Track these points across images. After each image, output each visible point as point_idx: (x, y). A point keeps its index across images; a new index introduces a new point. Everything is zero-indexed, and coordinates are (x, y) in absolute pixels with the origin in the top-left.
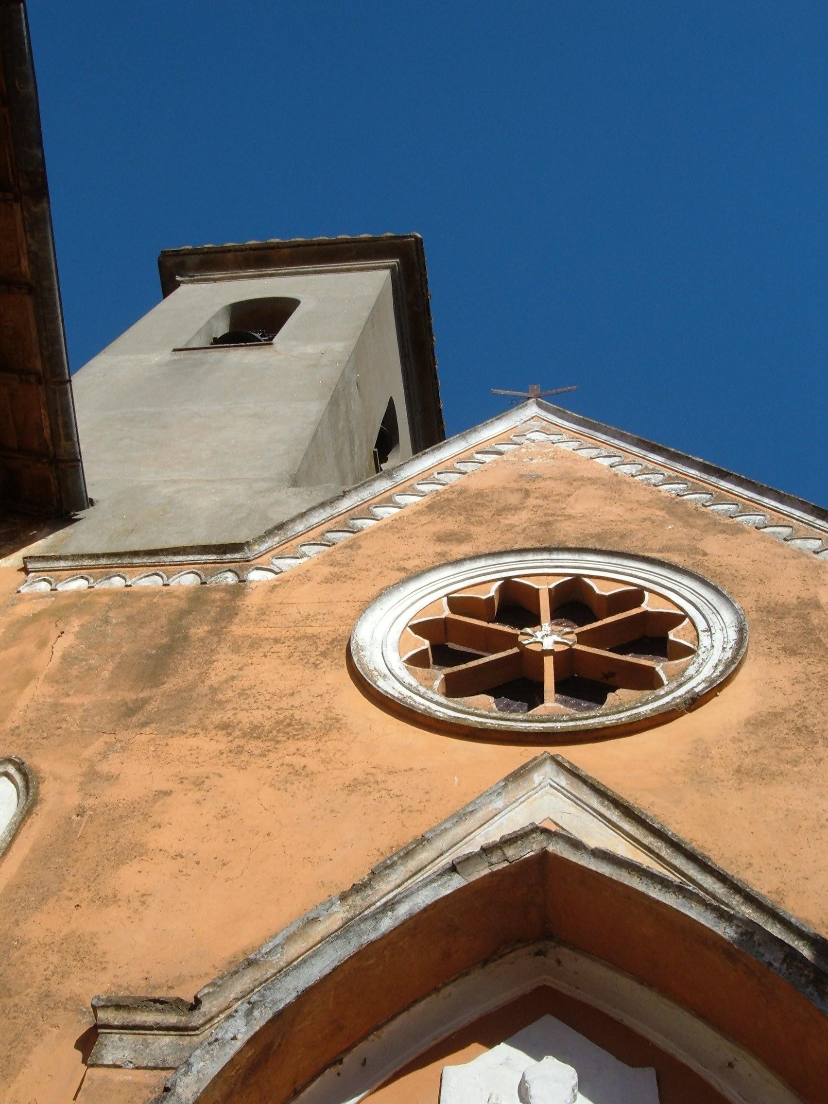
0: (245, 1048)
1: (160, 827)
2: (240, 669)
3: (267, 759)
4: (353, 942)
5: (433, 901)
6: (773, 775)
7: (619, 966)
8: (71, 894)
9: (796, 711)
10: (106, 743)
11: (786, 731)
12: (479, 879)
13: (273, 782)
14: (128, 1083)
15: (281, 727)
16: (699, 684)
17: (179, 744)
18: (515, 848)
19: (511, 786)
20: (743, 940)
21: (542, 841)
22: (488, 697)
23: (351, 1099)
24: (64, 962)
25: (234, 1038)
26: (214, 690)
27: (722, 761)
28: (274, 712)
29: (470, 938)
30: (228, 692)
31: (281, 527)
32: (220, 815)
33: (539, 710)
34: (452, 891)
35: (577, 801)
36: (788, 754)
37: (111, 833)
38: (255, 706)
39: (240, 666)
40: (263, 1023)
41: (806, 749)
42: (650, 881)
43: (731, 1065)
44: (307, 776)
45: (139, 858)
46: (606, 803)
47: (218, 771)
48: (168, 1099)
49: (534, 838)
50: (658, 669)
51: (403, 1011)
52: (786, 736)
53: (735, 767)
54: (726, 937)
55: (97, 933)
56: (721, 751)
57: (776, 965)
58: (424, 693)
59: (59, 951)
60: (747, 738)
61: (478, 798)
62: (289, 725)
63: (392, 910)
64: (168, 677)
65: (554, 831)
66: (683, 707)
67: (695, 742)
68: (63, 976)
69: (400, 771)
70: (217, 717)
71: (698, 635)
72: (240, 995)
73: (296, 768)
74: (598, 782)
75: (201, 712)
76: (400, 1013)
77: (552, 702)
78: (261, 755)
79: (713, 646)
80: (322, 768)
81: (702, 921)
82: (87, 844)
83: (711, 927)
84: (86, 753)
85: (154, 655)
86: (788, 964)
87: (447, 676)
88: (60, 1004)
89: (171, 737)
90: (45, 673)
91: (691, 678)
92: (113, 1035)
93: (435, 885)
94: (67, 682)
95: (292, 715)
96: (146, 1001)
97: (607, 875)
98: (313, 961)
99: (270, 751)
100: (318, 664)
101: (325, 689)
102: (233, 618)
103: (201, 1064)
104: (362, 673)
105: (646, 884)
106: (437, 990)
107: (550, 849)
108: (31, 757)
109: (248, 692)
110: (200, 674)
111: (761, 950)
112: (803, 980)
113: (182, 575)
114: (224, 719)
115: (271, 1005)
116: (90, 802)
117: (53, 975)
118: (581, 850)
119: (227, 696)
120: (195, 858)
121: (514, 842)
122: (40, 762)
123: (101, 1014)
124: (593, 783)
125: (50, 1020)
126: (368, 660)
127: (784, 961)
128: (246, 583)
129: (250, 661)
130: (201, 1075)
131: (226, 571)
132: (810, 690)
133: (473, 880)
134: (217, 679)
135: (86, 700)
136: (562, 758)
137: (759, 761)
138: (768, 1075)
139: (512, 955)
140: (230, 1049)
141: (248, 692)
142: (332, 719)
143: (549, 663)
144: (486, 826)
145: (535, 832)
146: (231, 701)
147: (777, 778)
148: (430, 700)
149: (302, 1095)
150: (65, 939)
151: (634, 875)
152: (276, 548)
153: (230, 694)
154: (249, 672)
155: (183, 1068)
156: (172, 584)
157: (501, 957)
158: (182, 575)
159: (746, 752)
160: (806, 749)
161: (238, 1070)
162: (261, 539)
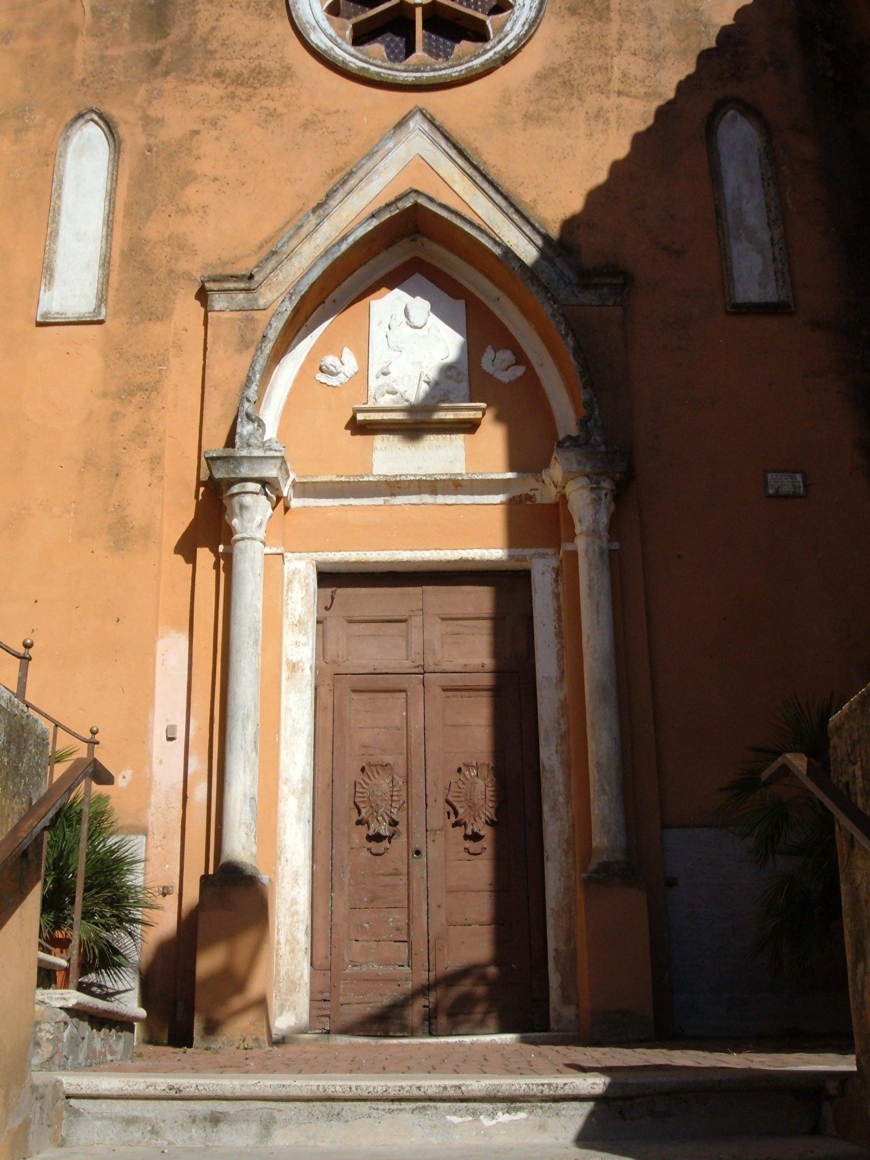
3: (250, 103)
14: (229, 319)
16: (511, 41)
19: (398, 132)
25: (286, 310)
33: (413, 59)
35: (434, 141)
40: (297, 302)
46: (449, 144)
50: (488, 22)
54: (497, 253)
58: (268, 1124)
61: (379, 142)
62: (259, 73)
63: (346, 240)
66: (499, 63)
68: (176, 260)
70: (213, 66)
72: (271, 271)
79: (524, 5)
80: (285, 111)
91: (506, 36)
93: (365, 225)
106: (365, 263)
107: (419, 201)
110: (191, 25)
114: (217, 68)
116: (152, 141)
122: (115, 111)
126: (302, 13)
136: (426, 111)
143: (419, 12)
148: (345, 51)
149: (309, 320)
150: (170, 237)
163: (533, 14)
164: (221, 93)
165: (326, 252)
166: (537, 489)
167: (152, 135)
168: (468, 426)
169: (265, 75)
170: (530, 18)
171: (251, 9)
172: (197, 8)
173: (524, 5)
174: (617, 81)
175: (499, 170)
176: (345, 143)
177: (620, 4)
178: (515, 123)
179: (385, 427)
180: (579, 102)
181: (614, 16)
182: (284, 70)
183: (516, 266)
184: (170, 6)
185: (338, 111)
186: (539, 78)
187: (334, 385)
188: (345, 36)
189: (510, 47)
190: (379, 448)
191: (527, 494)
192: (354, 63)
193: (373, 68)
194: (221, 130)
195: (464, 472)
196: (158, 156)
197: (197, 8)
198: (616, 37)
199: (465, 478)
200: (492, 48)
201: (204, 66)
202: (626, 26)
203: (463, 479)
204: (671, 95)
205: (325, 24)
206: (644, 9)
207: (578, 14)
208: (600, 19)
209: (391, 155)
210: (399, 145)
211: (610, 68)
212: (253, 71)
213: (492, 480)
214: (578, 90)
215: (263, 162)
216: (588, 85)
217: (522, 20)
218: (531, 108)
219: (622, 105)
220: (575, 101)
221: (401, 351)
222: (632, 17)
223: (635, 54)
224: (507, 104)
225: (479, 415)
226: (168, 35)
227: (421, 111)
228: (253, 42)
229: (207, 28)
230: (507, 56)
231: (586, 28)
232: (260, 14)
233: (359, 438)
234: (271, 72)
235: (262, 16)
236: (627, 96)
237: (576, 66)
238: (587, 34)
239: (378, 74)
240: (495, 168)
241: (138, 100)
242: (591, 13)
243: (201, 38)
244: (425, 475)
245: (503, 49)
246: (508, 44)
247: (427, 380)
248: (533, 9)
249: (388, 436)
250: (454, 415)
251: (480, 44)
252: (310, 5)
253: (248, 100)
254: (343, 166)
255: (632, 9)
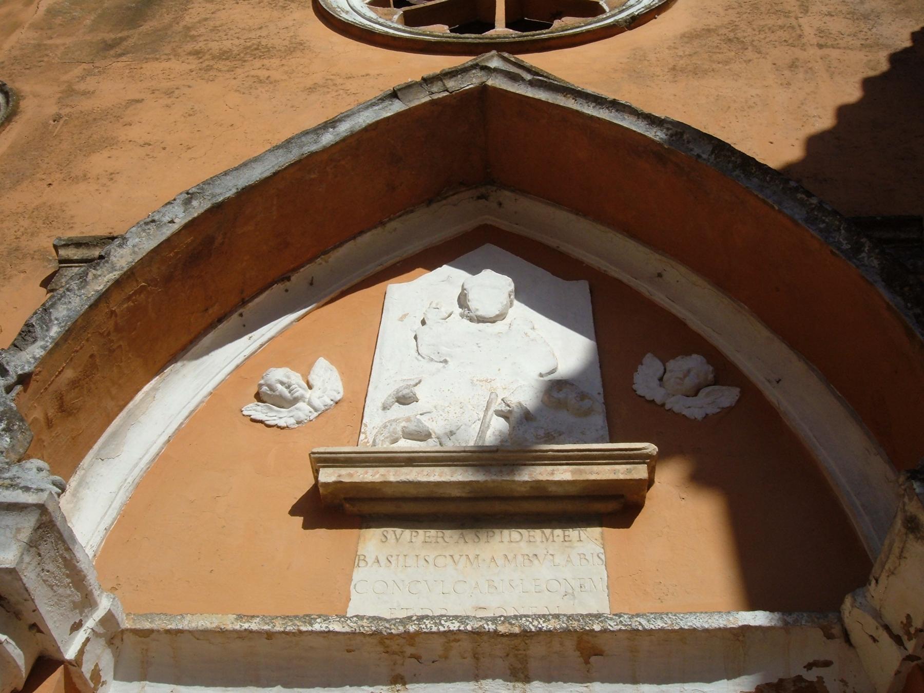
0: (183, 231)
1: (131, 125)
2: (213, 13)
3: (233, 73)
4: (294, 151)
5: (374, 121)
6: (705, 72)
7: (557, 201)
8: (44, 177)
9: (728, 28)
10: (84, 69)
11: (718, 41)
12: (419, 105)
13: (239, 89)
15: (248, 51)
17: (152, 68)
18: (455, 81)
20: (673, 140)
21: (481, 77)
22: (442, 25)
23: (298, 311)
24: (34, 225)
25: (172, 222)
26: (188, 28)
27: (659, 63)
28: (242, 41)
29: (413, 173)
30: (201, 29)
34: (392, 114)
37: (84, 131)
38: (225, 37)
39: (212, 11)
40: (201, 211)
41: (737, 53)
42: (585, 101)
43: (660, 275)
44: (271, 83)
45: (109, 148)
47: (188, 84)
48: (101, 265)
49: (474, 74)
51: (350, 240)
53: (671, 66)
54: (657, 139)
55: (66, 202)
56: (658, 55)
57: (704, 156)
59: (29, 217)
60: (682, 46)
62: (256, 49)
63: (334, 127)
64: (145, 22)
65: (493, 68)
67: (634, 50)
69: (358, 76)
70: (189, 47)
73: (261, 78)
74: (541, 70)
75: (174, 44)
76: (346, 241)
77: (502, 28)
78: (228, 71)
80: (285, 77)
81: (634, 128)
82: (62, 140)
83: (642, 132)
84: (65, 78)
85: (134, 7)
86: (716, 155)
88: (28, 255)
89: (146, 62)
90: (29, 22)
92: (73, 268)
93: (376, 108)
94: (50, 29)
95: (260, 43)
96: (105, 239)
97: (543, 99)
98: (254, 165)
99: (237, 67)
100: (284, 7)
101: (291, 23)
103: (137, 240)
104: (326, 8)
105: (581, 104)
106: (382, 224)
107: (490, 83)
108: (14, 82)
109: (220, 28)
111: (691, 146)
112: (730, 165)
115: (209, 198)
116: (65, 111)
117: (23, 234)
118: (519, 81)
119: (200, 32)
120: (163, 145)
121: (454, 76)
123: (63, 253)
124: (537, 71)
125: (18, 267)
127: (712, 152)
129: (223, 7)
130: (136, 249)
132: (742, 14)
133: (414, 105)
134: (191, 20)
135: (68, 41)
137: (693, 62)
138: (695, 278)
139: (456, 196)
140: (167, 230)
141: (220, 28)
142: (297, 44)
145: (475, 68)
146: (204, 35)
147: (709, 74)
149: (250, 305)
150: (37, 208)
151: (569, 98)
153: (202, 30)
155: (118, 241)
157: (445, 198)
159: (681, 56)
160: (737, 53)
161: (177, 253)
165: (287, 144)
166: (827, 664)
168: (611, 506)
179: (390, 508)
183: (704, 152)
187: (282, 423)
190: (370, 559)
191: (799, 678)
195: (606, 610)
199: (612, 625)
203: (605, 631)
213: (694, 631)
221: (446, 361)
225: (640, 472)
233: (322, 535)
244: (494, 620)
247: (504, 408)
249: (398, 531)
250: (573, 472)
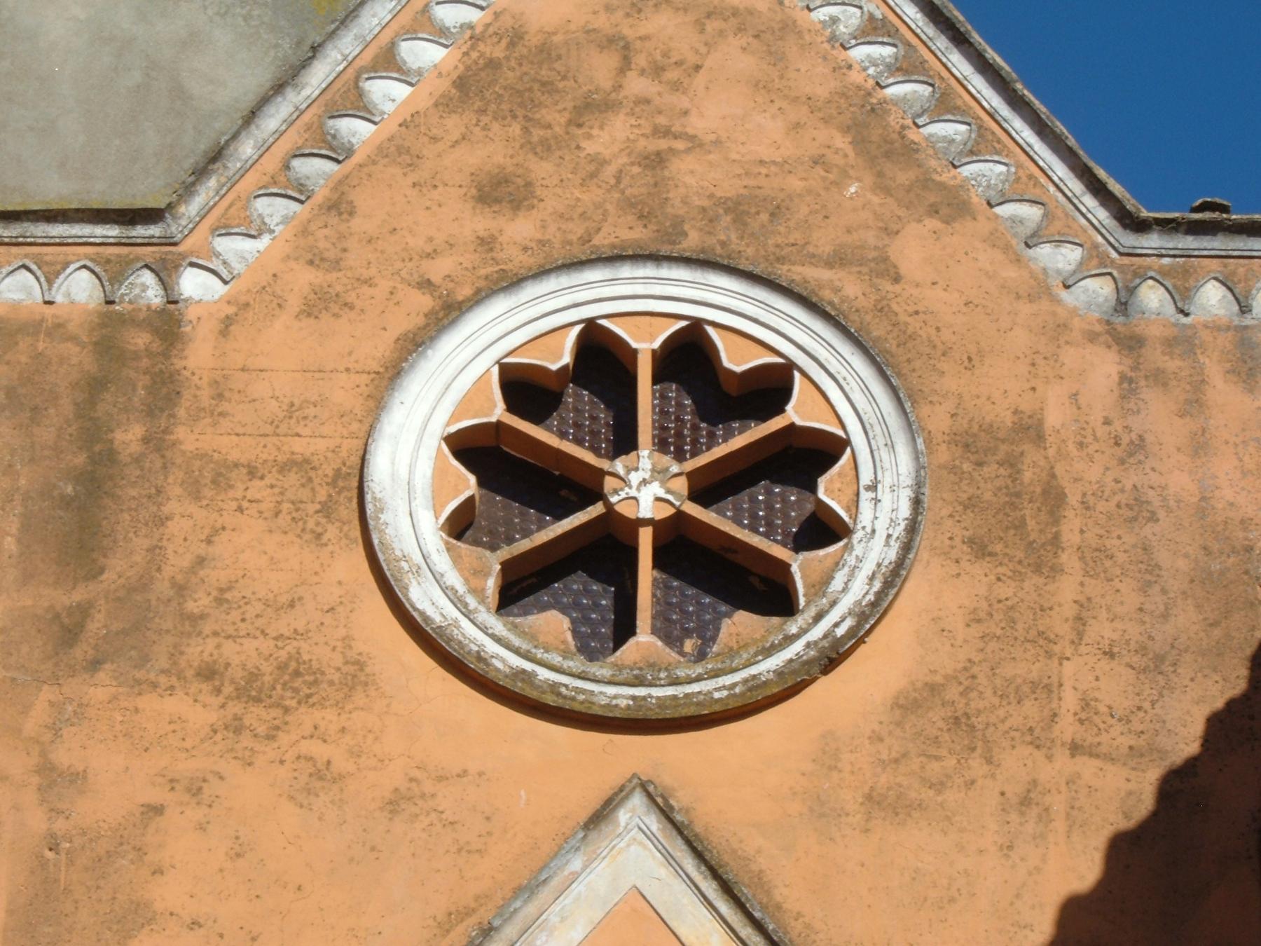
3: (276, 745)
16: (843, 619)
19: (593, 835)
31: (216, 155)
32: (233, 852)
33: (631, 651)
35: (669, 858)
36: (934, 768)
45: (147, 928)
46: (703, 868)
50: (795, 568)
52: (939, 733)
62: (297, 673)
70: (198, 651)
71: (858, 494)
80: (351, 767)
87: (507, 566)
91: (834, 603)
102: (175, 405)
110: (151, 550)
113: (71, 274)
114: (206, 656)
116: (60, 825)
128: (180, 305)
131: (142, 267)
137: (898, 780)
144: (561, 898)
148: (484, 629)
152: (215, 204)
154: (222, 547)
156: (59, 299)
158: (71, 274)
159: (884, 761)
162: (187, 190)
163: (892, 554)
164: (212, 717)
167: (60, 812)
169: (310, 678)
170: (886, 562)
171: (284, 520)
172: (166, 510)
173: (874, 531)
174: (1070, 718)
175: (808, 926)
176: (479, 851)
177: (1082, 532)
178: (847, 815)
180: (986, 768)
181: (1068, 559)
182: (351, 669)
184: (107, 501)
185: (464, 773)
186: (901, 707)
188: (483, 590)
189: (840, 632)
192: (504, 660)
193: (544, 674)
194: (210, 806)
196: (71, 862)
197: (166, 510)
198: (1070, 611)
200: (803, 631)
201: (175, 653)
202: (1094, 588)
204: (1191, 748)
205: (442, 562)
206: (1134, 546)
207: (990, 554)
208: (1038, 569)
209: (577, 888)
210: (593, 865)
211: (1055, 689)
212: (282, 667)
214: (986, 741)
215: (299, 888)
216: (1008, 724)
217: (868, 568)
218: (883, 779)
219: (1079, 775)
220: (976, 765)
222: (1108, 563)
223: (1110, 655)
224: (831, 768)
226: (102, 570)
227: (643, 786)
228: (284, 599)
229: (186, 561)
230: (834, 656)
231: (1006, 590)
232: (303, 530)
234: (323, 673)
235: (307, 536)
236: (1091, 755)
237: (982, 679)
238: (1009, 603)
239: (554, 687)
240: (801, 920)
241: (31, 726)
242: (1020, 555)
243: (174, 583)
245: (825, 636)
246: (837, 625)
248: (892, 543)
251: (775, 620)
252: (411, 514)
253: (271, 738)
254: (473, 905)
255: (1108, 543)
